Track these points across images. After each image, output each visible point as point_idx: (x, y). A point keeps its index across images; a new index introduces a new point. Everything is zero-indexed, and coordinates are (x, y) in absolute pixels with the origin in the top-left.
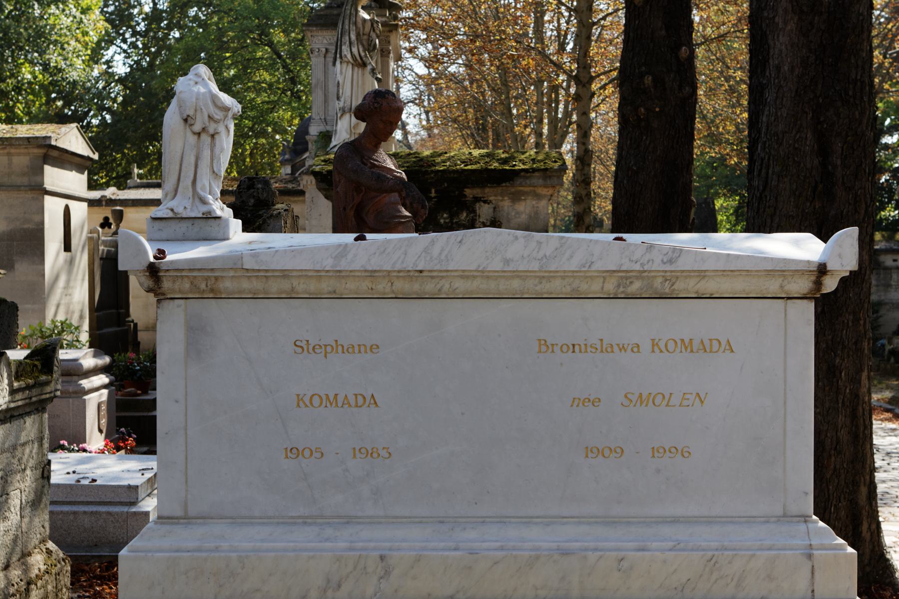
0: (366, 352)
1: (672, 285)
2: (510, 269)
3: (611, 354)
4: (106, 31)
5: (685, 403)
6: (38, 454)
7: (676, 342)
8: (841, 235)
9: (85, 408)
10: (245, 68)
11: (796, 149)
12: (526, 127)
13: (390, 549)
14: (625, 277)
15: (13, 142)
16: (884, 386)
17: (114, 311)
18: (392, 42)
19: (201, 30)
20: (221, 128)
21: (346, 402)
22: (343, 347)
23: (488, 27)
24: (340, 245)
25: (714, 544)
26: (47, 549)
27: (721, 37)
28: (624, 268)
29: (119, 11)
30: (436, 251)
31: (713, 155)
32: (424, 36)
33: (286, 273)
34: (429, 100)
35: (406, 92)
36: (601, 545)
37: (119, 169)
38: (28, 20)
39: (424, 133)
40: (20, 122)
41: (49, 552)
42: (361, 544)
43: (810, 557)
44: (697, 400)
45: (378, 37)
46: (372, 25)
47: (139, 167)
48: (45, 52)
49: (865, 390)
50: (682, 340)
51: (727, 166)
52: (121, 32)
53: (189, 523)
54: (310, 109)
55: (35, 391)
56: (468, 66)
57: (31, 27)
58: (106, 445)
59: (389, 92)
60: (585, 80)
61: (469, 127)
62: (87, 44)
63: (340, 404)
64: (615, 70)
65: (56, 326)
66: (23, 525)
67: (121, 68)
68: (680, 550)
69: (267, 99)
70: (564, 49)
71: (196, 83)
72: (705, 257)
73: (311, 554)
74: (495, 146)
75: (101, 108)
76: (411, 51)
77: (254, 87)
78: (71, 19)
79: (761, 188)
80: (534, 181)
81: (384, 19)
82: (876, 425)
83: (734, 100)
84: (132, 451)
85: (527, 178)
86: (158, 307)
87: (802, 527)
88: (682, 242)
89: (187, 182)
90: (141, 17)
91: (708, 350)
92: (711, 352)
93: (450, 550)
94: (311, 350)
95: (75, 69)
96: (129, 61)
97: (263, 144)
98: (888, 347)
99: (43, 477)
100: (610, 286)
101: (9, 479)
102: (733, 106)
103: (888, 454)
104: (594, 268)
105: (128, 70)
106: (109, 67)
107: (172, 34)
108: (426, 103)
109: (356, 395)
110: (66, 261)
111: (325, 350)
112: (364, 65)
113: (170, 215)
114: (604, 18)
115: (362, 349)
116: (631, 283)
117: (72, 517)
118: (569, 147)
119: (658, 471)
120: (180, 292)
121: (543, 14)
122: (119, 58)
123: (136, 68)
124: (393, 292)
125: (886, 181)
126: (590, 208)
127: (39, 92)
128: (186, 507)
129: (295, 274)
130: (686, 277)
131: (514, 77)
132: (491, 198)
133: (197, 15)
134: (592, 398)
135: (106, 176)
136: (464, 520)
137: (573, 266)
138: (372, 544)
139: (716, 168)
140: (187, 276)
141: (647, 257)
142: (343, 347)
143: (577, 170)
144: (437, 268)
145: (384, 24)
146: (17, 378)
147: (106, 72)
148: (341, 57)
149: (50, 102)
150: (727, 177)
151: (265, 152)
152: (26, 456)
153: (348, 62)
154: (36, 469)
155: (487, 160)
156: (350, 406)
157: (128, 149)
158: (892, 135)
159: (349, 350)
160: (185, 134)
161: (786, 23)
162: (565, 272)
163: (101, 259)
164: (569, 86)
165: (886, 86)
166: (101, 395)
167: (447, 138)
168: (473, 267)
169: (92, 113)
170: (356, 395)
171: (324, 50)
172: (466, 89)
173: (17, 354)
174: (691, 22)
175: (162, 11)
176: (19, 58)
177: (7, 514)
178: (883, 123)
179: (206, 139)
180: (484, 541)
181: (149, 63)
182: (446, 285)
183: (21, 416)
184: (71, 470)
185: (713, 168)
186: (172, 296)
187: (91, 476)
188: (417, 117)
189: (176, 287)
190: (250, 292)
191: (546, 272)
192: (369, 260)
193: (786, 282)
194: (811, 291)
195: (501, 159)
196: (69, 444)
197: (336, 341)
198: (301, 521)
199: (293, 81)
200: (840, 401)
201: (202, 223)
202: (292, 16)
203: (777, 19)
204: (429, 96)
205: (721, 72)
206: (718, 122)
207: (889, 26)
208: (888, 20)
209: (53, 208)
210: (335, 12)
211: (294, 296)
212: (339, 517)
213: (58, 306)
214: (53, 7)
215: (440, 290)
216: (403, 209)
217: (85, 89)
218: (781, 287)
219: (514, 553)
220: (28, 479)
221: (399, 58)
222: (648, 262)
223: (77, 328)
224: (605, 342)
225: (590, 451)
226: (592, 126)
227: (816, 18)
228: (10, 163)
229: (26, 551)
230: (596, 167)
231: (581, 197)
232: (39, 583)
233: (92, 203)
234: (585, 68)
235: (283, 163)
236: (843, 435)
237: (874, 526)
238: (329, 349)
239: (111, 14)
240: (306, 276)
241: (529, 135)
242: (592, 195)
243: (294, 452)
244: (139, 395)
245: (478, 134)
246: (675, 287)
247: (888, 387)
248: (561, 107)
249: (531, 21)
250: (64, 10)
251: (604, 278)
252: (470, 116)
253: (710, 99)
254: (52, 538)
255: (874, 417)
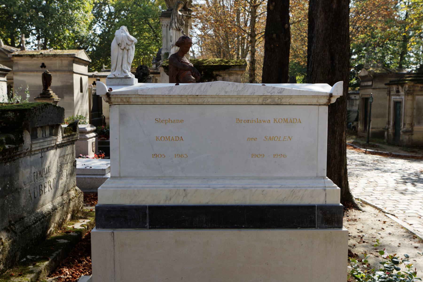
0: (179, 122)
1: (281, 100)
2: (227, 95)
3: (261, 124)
4: (94, 19)
5: (285, 140)
6: (72, 158)
7: (282, 119)
8: (337, 84)
9: (88, 144)
10: (140, 32)
11: (323, 58)
12: (234, 52)
13: (187, 187)
14: (265, 97)
15: (63, 56)
16: (350, 138)
17: (97, 112)
18: (189, 22)
19: (125, 19)
20: (131, 48)
21: (173, 139)
22: (171, 121)
23: (221, 18)
24: (170, 87)
25: (294, 186)
26: (75, 189)
27: (299, 21)
28: (265, 95)
29: (98, 12)
30: (202, 88)
31: (296, 61)
32: (199, 21)
33: (152, 96)
34: (202, 43)
35: (194, 40)
36: (257, 186)
37: (99, 65)
38: (67, 15)
39: (200, 54)
40: (65, 49)
41: (76, 190)
42: (178, 186)
43: (325, 190)
44: (289, 139)
45: (184, 21)
46: (182, 17)
47: (105, 65)
48: (73, 26)
49: (344, 138)
50: (284, 119)
51: (300, 65)
52: (99, 19)
53: (121, 179)
54: (162, 46)
55: (70, 137)
56: (214, 31)
57: (68, 17)
58: (95, 156)
59: (187, 37)
60: (253, 36)
61: (215, 52)
62: (87, 23)
63: (171, 140)
64: (263, 32)
65: (78, 117)
66: (68, 181)
67: (99, 32)
68: (282, 188)
69: (147, 42)
70: (247, 26)
71: (122, 32)
72: (291, 91)
73: (161, 189)
74: (223, 58)
75: (92, 45)
76: (195, 26)
77: (143, 38)
78: (82, 15)
79: (311, 71)
80: (236, 69)
81: (186, 15)
82: (348, 151)
83: (303, 43)
84: (104, 158)
85: (234, 68)
86: (110, 107)
87: (323, 180)
88: (285, 86)
89: (119, 66)
90: (105, 14)
91: (293, 122)
92: (294, 123)
93: (207, 187)
94: (161, 122)
95: (84, 32)
96: (102, 29)
97: (147, 58)
98: (352, 125)
99: (74, 166)
100: (260, 101)
101: (63, 166)
102: (303, 45)
103: (351, 160)
104: (255, 95)
105: (101, 32)
106: (95, 31)
107: (116, 20)
108: (201, 44)
109: (176, 137)
110: (81, 96)
111: (166, 122)
112: (180, 30)
113: (114, 77)
114: (260, 15)
115: (178, 121)
116: (267, 100)
117: (84, 179)
118: (248, 59)
119: (276, 162)
120: (117, 102)
121: (239, 13)
122: (98, 28)
123: (104, 32)
124: (188, 102)
125: (353, 70)
126: (255, 79)
127: (72, 39)
128: (120, 174)
129: (155, 96)
130: (286, 98)
131: (230, 35)
132: (222, 75)
133: (124, 14)
134: (254, 138)
135: (94, 68)
136: (211, 178)
137: (248, 94)
138: (181, 186)
139: (297, 66)
140: (119, 97)
141: (273, 91)
142: (171, 121)
143: (251, 66)
144: (203, 94)
145: (186, 16)
146: (65, 133)
147: (94, 33)
148: (172, 27)
149: (75, 43)
150: (300, 69)
151: (147, 60)
152: (68, 159)
153: (174, 29)
154: (71, 163)
155: (221, 62)
156: (174, 140)
157: (102, 59)
158: (355, 55)
159: (174, 122)
160: (118, 49)
161: (320, 15)
162: (245, 96)
163: (93, 95)
164: (248, 38)
165: (354, 38)
166: (93, 140)
167: (207, 56)
168: (215, 94)
169: (89, 47)
170: (176, 137)
171: (166, 25)
172: (214, 39)
173: (64, 126)
174: (289, 16)
175: (112, 12)
176: (65, 28)
177: (62, 177)
178: (352, 51)
179: (125, 51)
180: (218, 185)
181: (108, 30)
182: (206, 100)
183: (66, 145)
184: (83, 164)
185: (296, 66)
186: (115, 104)
187: (90, 166)
188: (198, 49)
189: (116, 100)
190: (141, 102)
191: (239, 96)
192: (180, 92)
193: (319, 100)
194: (327, 103)
195: (225, 62)
196: (83, 156)
197: (169, 119)
198: (158, 178)
199: (156, 36)
200: (336, 142)
201: (124, 79)
202: (156, 14)
203: (317, 14)
204: (202, 41)
205: (299, 34)
206: (297, 50)
207: (355, 18)
208: (355, 16)
209: (76, 78)
210: (170, 12)
211: (155, 104)
212: (170, 177)
213: (79, 111)
214: (76, 11)
215: (204, 102)
216: (192, 77)
217: (87, 38)
218: (317, 101)
219: (228, 189)
220: (69, 166)
221: (191, 28)
222: (273, 92)
223: (85, 118)
224: (258, 120)
225: (253, 155)
226: (255, 51)
227: (331, 14)
228: (62, 63)
229: (68, 190)
230: (257, 66)
231: (252, 75)
232: (73, 200)
233: (90, 77)
234: (253, 31)
235: (153, 64)
236: (337, 153)
237: (346, 183)
238: (167, 121)
239: (95, 13)
240: (159, 97)
241: (235, 55)
242: (256, 75)
243: (155, 156)
244: (106, 140)
245: (218, 54)
246: (282, 101)
247: (352, 139)
248: (246, 45)
249: (235, 16)
250: (79, 12)
251: (258, 98)
252: (215, 48)
253: (295, 43)
254: (77, 186)
255: (347, 148)
